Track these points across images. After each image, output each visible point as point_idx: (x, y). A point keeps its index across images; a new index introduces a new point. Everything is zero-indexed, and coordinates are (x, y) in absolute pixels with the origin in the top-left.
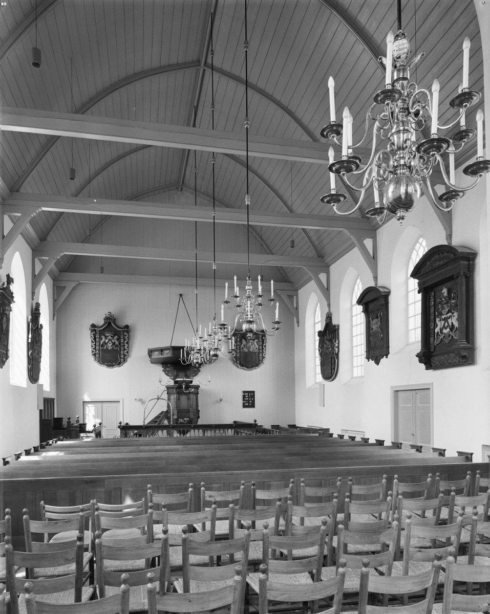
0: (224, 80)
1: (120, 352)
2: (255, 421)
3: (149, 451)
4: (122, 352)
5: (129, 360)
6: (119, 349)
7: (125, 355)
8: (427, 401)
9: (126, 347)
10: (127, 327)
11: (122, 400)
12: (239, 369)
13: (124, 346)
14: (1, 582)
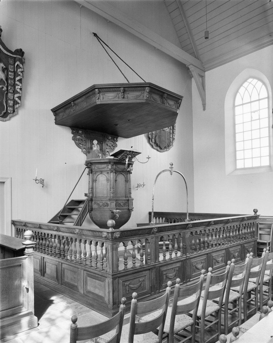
0: (255, 89)
1: (7, 94)
2: (255, 211)
3: (44, 266)
4: (10, 95)
5: (21, 112)
6: (5, 88)
7: (15, 103)
8: (21, 97)
9: (18, 88)
10: (20, 52)
11: (9, 180)
12: (153, 149)
13: (14, 85)
14: (131, 340)
